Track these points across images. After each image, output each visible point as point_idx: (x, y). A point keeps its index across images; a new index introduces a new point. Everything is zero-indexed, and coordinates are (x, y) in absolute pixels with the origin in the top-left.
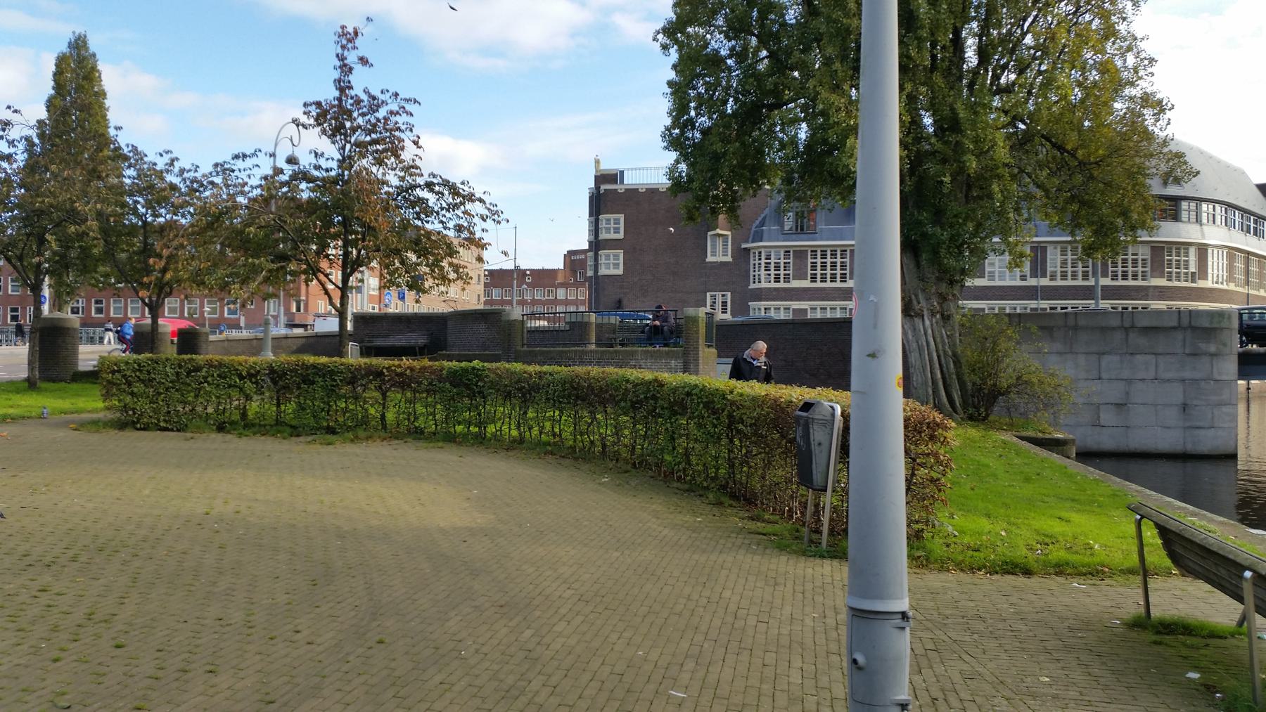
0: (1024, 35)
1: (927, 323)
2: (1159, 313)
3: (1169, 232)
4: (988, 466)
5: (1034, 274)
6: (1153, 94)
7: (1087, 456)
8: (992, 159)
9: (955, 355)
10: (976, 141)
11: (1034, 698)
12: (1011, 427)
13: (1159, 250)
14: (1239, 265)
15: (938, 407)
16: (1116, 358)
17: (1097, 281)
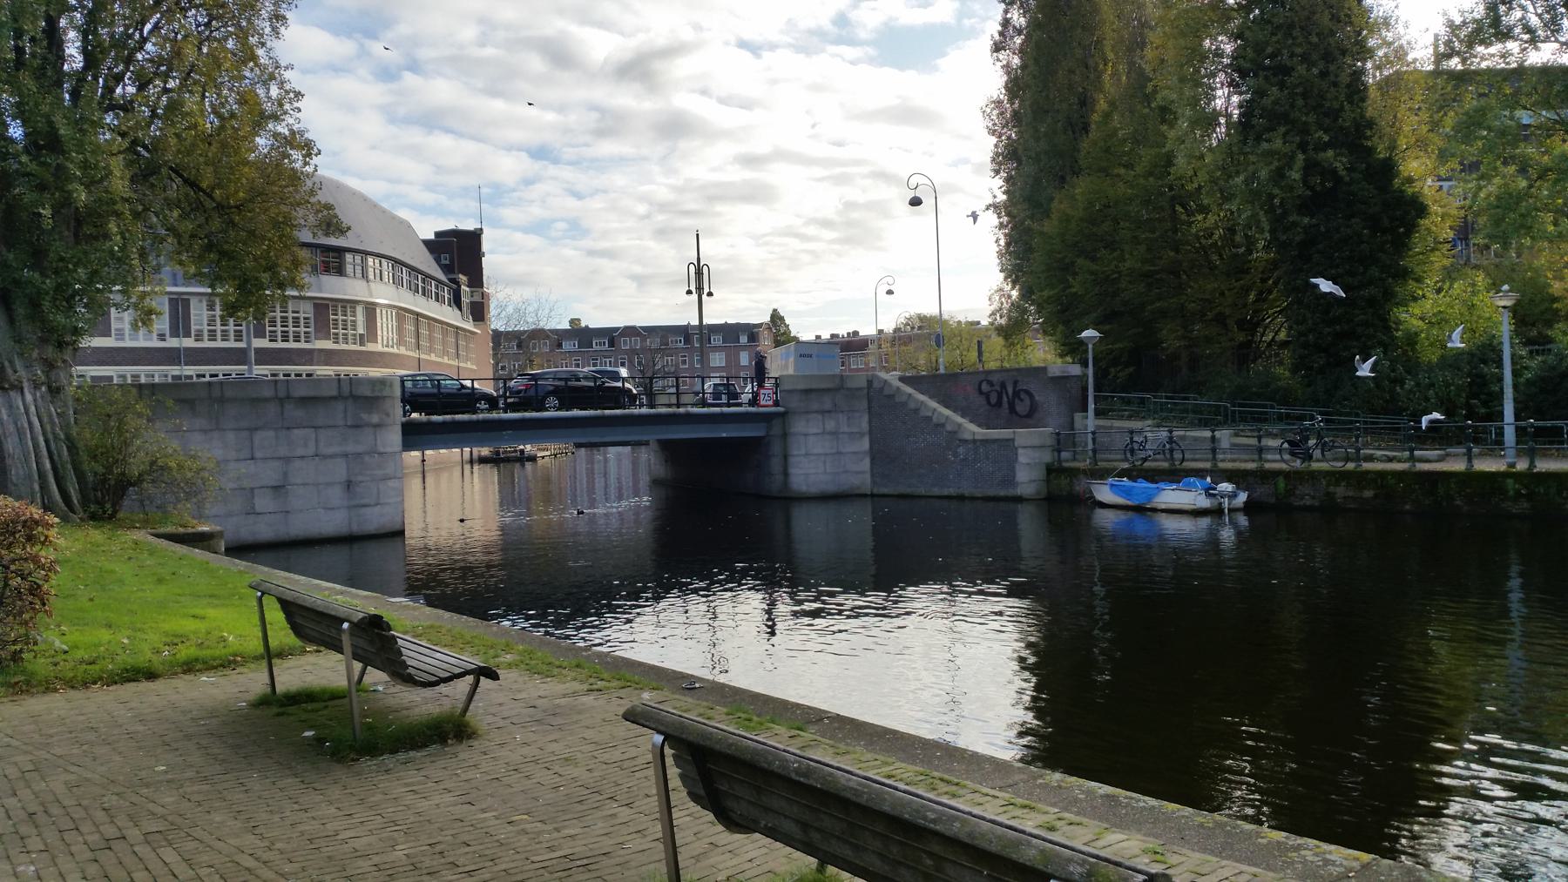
0: (144, 40)
1: (29, 397)
2: (326, 380)
3: (332, 287)
4: (112, 572)
5: (175, 332)
6: (302, 133)
7: (239, 550)
8: (107, 192)
9: (68, 438)
10: (85, 166)
11: (147, 786)
12: (146, 523)
13: (324, 310)
14: (410, 327)
15: (47, 507)
16: (271, 433)
17: (249, 343)
